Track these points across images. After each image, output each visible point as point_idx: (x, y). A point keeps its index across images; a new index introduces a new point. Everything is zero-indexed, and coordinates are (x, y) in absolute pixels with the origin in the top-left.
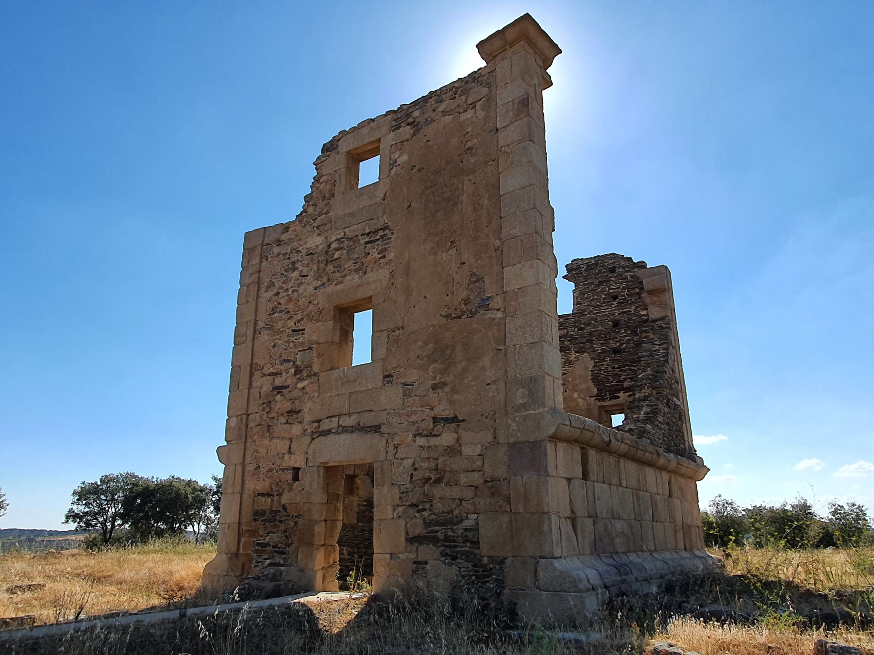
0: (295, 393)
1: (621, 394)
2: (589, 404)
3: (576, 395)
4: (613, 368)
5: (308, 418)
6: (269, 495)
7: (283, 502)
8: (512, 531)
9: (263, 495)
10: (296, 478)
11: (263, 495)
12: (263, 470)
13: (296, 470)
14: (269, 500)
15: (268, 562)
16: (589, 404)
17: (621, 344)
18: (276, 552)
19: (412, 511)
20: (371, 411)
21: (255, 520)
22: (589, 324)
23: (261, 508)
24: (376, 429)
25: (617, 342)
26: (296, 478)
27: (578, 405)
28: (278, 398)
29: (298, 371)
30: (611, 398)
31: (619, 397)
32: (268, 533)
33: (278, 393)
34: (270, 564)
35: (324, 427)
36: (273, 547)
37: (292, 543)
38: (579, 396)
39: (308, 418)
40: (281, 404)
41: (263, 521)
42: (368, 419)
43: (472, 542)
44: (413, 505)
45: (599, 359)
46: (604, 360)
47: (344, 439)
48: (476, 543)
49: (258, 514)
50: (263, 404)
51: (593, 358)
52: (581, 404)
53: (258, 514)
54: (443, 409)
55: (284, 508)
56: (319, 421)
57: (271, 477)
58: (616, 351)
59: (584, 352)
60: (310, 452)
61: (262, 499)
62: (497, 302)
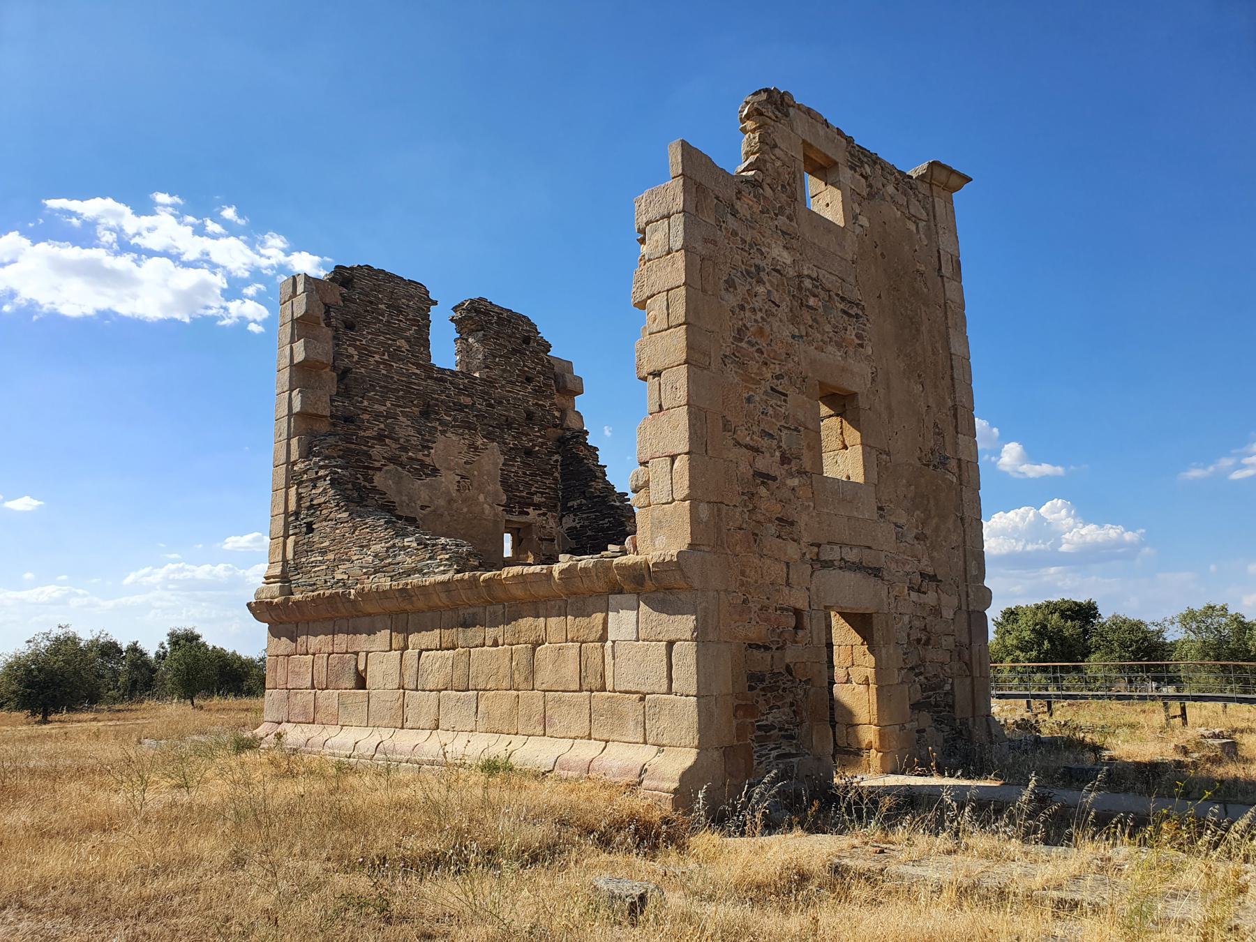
0: (785, 493)
1: (530, 510)
2: (496, 515)
3: (481, 498)
4: (524, 473)
5: (806, 539)
6: (767, 648)
7: (788, 661)
8: (1130, 697)
9: (758, 647)
10: (799, 626)
11: (758, 647)
12: (755, 607)
13: (798, 613)
14: (768, 655)
15: (774, 753)
16: (496, 515)
17: (534, 446)
18: (784, 737)
19: (912, 675)
20: (869, 548)
21: (751, 688)
22: (500, 403)
23: (758, 669)
24: (876, 572)
25: (531, 440)
26: (799, 626)
27: (483, 513)
28: (763, 491)
29: (785, 460)
30: (520, 513)
31: (528, 514)
32: (771, 708)
33: (763, 483)
34: (778, 757)
35: (832, 554)
36: (780, 729)
37: (802, 722)
38: (486, 502)
39: (806, 539)
40: (768, 504)
41: (763, 689)
42: (869, 558)
43: (950, 706)
44: (912, 669)
45: (511, 454)
46: (514, 459)
47: (850, 577)
48: (952, 707)
49: (755, 679)
50: (743, 494)
51: (503, 453)
52: (487, 512)
53: (755, 679)
54: (926, 565)
55: (789, 670)
56: (819, 546)
57: (767, 620)
58: (529, 452)
59: (493, 440)
60: (813, 588)
61: (757, 654)
62: (953, 464)
